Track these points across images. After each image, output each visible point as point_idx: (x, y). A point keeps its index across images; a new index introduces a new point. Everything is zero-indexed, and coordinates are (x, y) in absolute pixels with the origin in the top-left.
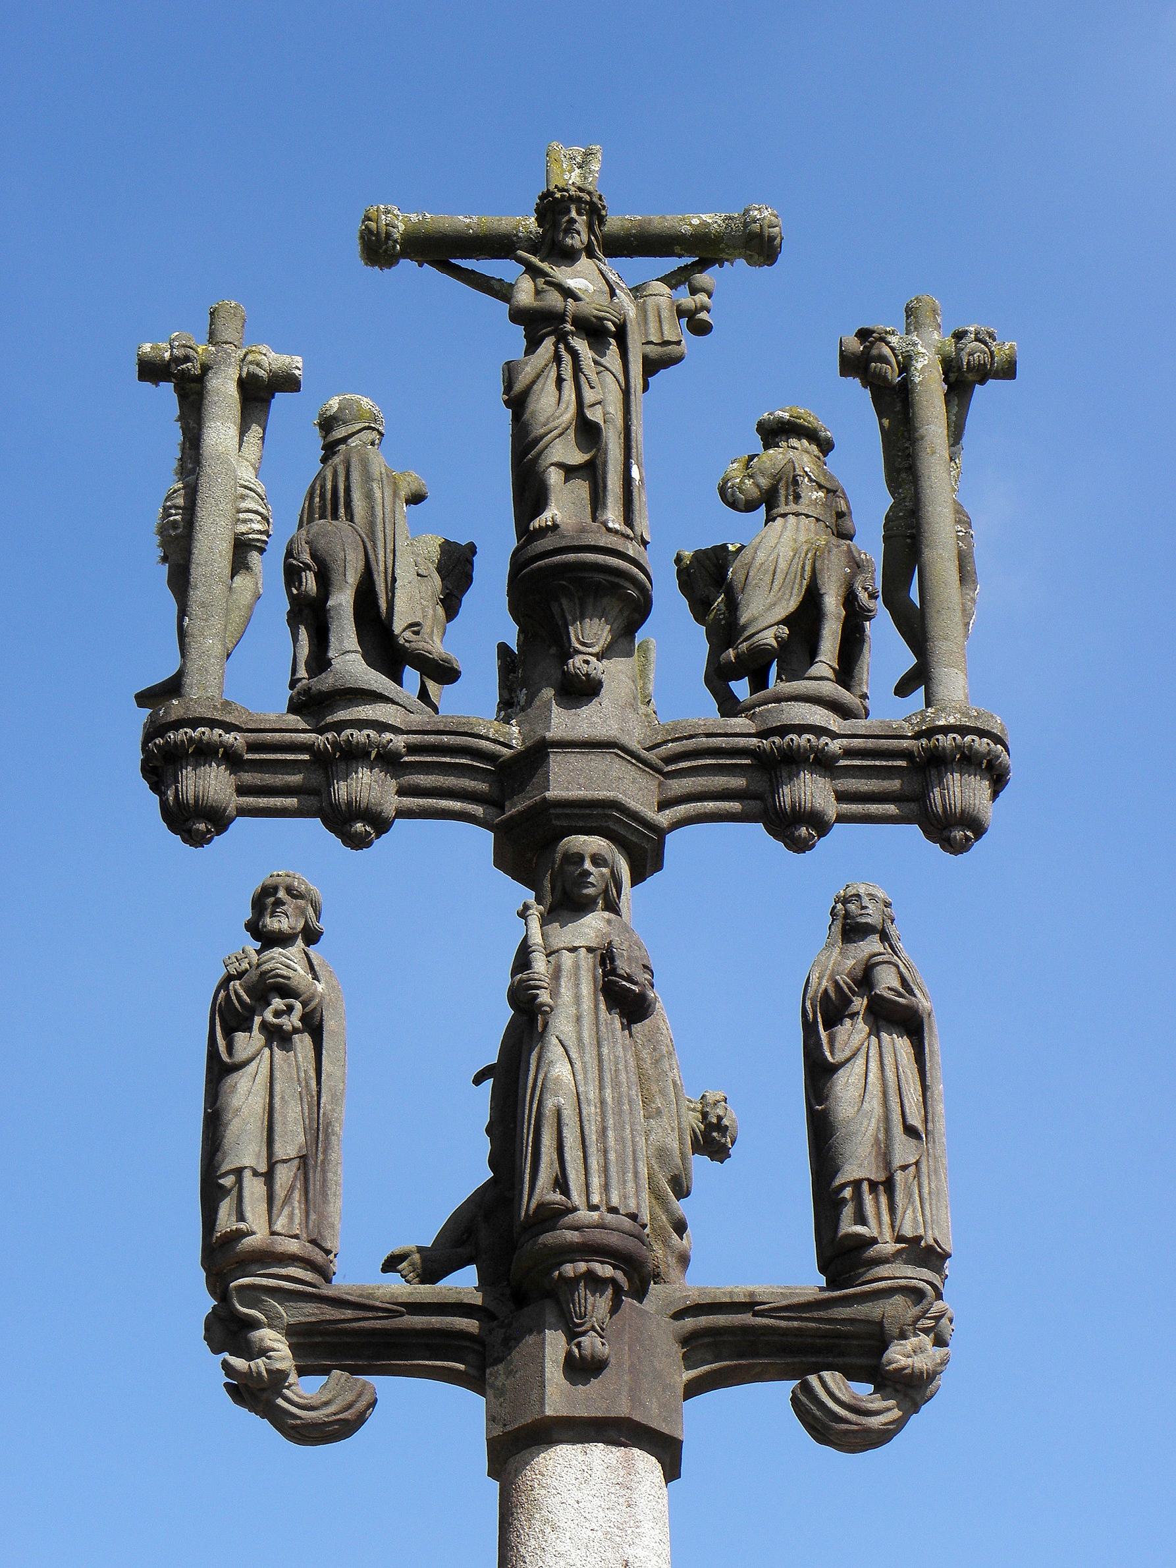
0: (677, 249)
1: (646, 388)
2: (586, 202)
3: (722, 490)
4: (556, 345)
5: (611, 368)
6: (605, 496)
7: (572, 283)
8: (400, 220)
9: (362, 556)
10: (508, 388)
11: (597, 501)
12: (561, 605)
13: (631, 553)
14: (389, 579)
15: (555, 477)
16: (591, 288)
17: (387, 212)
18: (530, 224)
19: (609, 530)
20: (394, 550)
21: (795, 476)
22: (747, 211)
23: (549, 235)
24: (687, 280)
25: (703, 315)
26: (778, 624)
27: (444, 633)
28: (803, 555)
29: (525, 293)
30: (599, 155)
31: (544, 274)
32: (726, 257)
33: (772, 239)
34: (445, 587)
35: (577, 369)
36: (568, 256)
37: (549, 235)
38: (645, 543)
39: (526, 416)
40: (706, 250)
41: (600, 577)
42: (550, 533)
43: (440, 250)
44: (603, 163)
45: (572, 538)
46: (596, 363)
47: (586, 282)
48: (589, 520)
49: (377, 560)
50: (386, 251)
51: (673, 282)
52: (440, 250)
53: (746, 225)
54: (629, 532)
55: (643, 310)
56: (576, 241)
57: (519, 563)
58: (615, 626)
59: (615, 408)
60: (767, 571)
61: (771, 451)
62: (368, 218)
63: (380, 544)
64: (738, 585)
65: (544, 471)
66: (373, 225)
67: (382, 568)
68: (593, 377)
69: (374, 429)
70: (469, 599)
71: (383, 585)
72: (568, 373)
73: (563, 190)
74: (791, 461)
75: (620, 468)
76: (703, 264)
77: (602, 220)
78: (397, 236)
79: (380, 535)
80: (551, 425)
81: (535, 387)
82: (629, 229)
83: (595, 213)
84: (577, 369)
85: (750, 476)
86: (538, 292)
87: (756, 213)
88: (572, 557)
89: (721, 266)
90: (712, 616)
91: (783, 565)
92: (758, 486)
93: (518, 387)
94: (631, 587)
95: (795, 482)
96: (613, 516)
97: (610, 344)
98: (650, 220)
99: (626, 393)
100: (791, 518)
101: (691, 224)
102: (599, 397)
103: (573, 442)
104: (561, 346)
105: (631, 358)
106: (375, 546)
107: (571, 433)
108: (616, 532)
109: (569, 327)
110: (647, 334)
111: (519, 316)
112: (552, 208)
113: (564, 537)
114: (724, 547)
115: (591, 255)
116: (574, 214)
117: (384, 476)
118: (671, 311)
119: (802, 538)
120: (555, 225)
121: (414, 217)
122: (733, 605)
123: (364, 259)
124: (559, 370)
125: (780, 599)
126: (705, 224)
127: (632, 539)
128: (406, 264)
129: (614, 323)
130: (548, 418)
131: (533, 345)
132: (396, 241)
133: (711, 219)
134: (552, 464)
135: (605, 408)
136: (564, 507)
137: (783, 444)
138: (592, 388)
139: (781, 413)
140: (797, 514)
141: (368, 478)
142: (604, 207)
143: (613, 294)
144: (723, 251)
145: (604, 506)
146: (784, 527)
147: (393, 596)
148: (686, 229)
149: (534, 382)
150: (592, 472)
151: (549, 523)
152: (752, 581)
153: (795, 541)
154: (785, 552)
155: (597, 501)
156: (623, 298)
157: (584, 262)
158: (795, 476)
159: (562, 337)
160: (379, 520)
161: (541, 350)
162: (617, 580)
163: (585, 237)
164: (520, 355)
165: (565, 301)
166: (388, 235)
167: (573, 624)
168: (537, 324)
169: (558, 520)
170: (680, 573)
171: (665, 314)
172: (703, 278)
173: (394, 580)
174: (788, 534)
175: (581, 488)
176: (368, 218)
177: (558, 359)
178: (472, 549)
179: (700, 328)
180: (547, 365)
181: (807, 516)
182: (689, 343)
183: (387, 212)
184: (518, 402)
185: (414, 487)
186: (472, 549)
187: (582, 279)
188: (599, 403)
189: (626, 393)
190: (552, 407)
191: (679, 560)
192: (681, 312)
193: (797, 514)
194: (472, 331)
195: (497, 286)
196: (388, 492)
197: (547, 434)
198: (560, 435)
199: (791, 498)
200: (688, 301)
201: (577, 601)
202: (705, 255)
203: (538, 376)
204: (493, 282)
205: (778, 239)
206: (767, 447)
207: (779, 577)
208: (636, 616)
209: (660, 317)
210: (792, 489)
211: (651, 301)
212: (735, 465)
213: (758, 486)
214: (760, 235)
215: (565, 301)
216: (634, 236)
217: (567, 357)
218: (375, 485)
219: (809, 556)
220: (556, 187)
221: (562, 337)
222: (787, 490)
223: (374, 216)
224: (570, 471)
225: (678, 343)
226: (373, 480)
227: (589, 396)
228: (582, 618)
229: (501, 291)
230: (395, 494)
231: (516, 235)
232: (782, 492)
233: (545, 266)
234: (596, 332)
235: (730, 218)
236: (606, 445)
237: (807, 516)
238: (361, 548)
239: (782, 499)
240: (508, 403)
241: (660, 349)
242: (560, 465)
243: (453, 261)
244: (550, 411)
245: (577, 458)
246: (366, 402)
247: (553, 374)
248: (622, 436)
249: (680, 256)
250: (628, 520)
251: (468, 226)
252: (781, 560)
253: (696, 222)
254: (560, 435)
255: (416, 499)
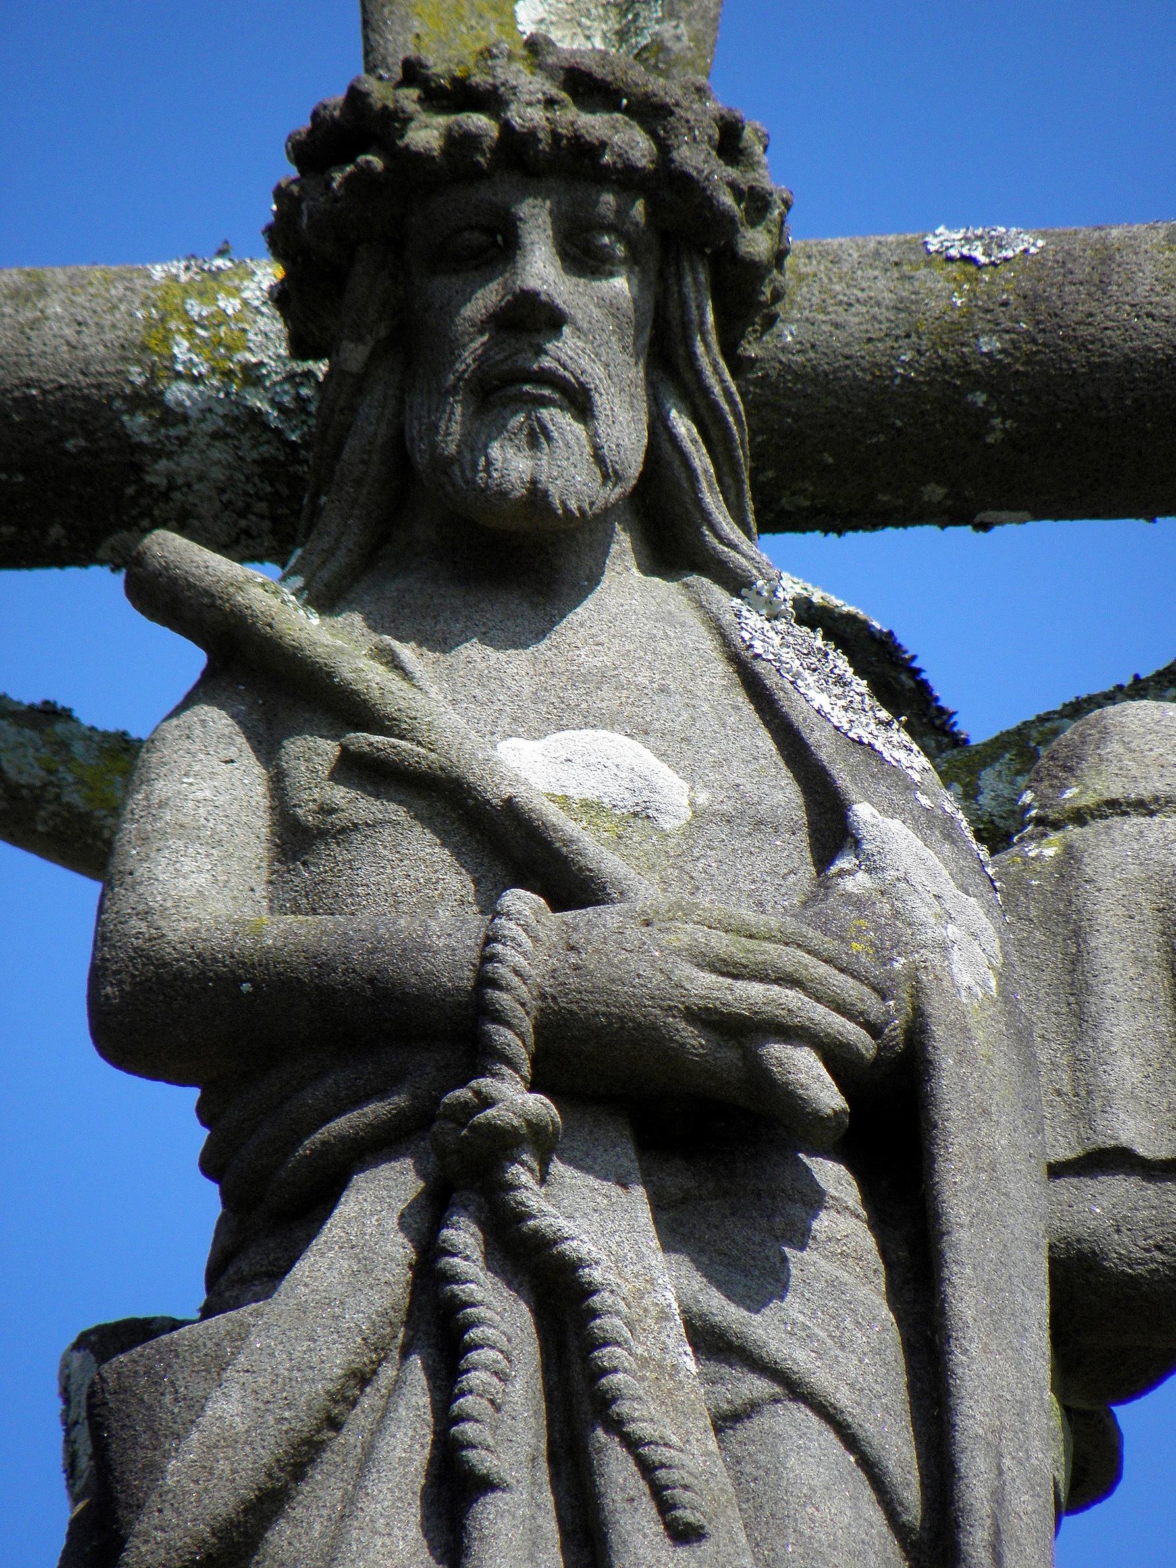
1: (1092, 1470)
2: (627, 179)
4: (426, 1224)
5: (822, 1379)
7: (533, 768)
16: (675, 796)
18: (225, 312)
29: (207, 849)
35: (578, 1400)
36: (516, 569)
46: (710, 1341)
55: (1055, 931)
56: (565, 462)
68: (692, 1454)
73: (459, 95)
77: (744, 296)
82: (956, 330)
83: (693, 245)
84: (578, 1400)
86: (296, 838)
97: (815, 1200)
98: (1105, 256)
104: (464, 1236)
109: (514, 1099)
110: (1085, 1099)
111: (153, 1012)
112: (392, 219)
115: (673, 546)
116: (541, 268)
120: (412, 345)
124: (445, 1417)
129: (836, 1057)
131: (266, 1220)
138: (684, 1534)
142: (757, 204)
143: (831, 831)
156: (910, 845)
159: (468, 1176)
161: (321, 1266)
163: (624, 428)
165: (489, 906)
177: (437, 1327)
180: (362, 1378)
187: (619, 725)
203: (302, 1458)
215: (489, 906)
216: (995, 376)
217: (502, 1319)
220: (413, 73)
221: (468, 1176)
233: (338, 641)
234: (699, 1118)
247: (407, 1445)
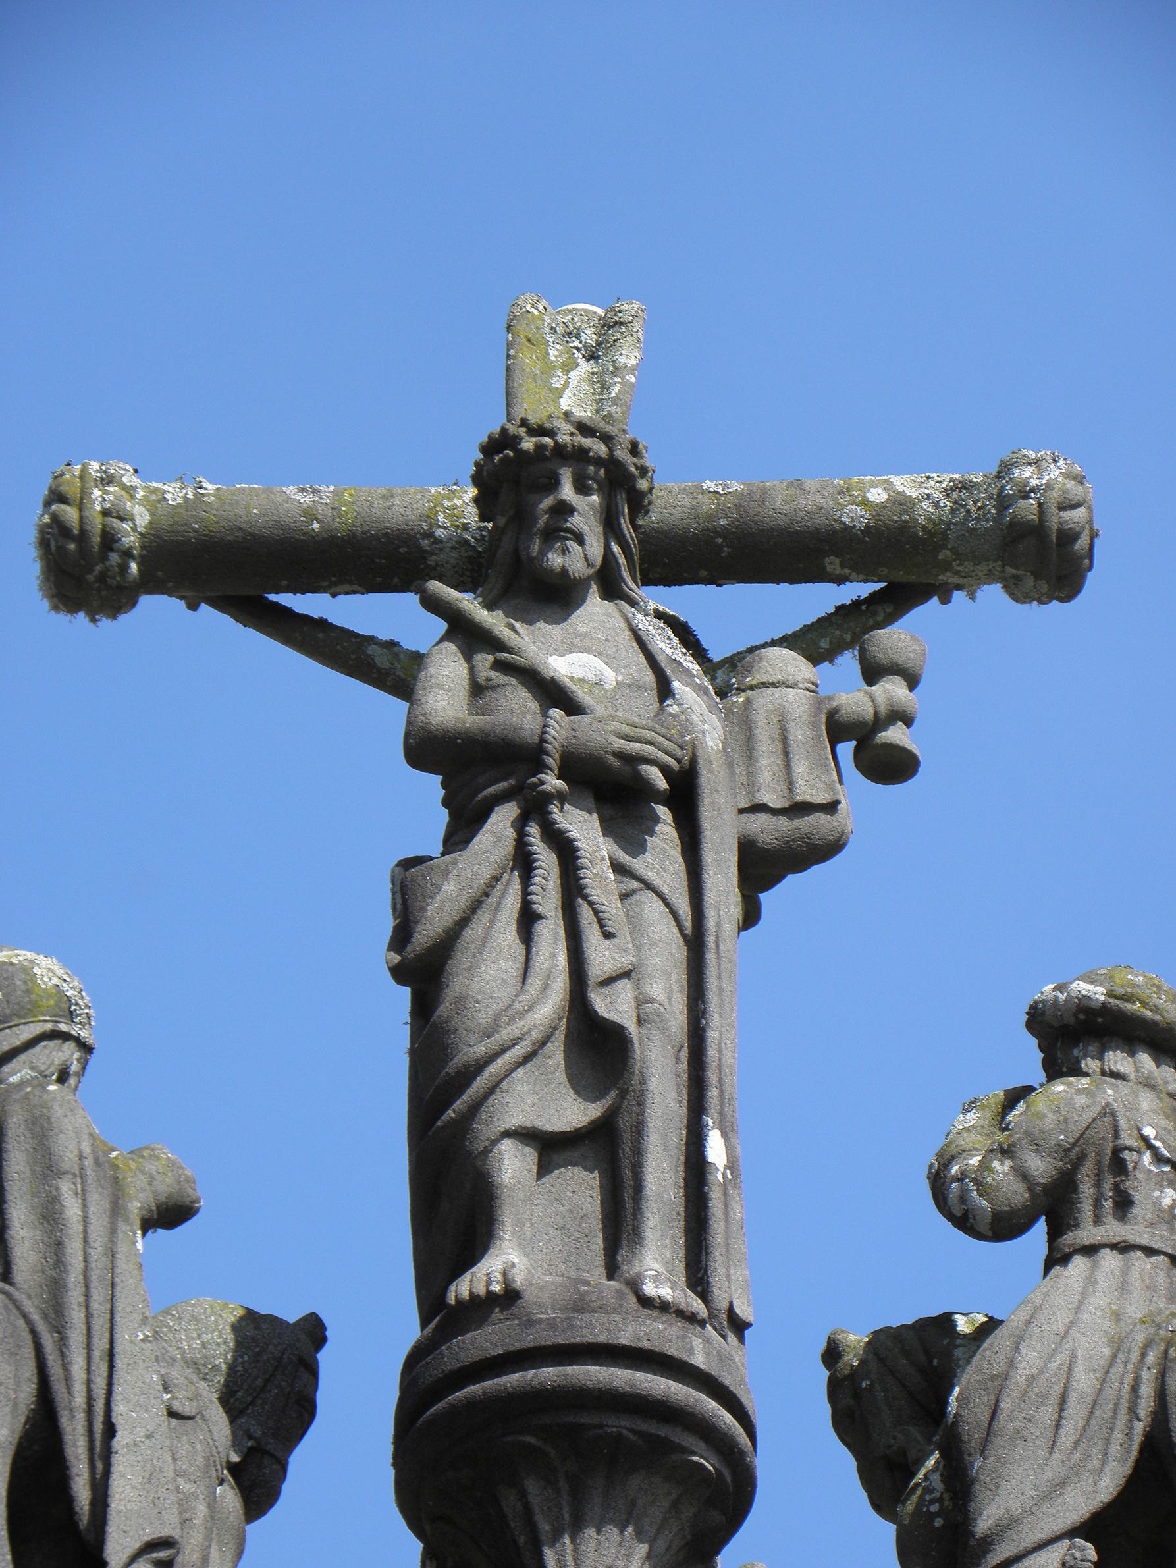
0: (832, 564)
1: (751, 916)
2: (598, 461)
3: (938, 1182)
4: (520, 825)
6: (637, 1211)
7: (564, 666)
8: (140, 496)
9: (29, 1370)
10: (401, 937)
11: (619, 1224)
12: (523, 1494)
13: (699, 1360)
14: (98, 1427)
15: (512, 1165)
16: (610, 677)
17: (107, 480)
18: (457, 505)
19: (646, 1302)
20: (111, 1355)
21: (1117, 1151)
22: (1005, 468)
23: (507, 544)
24: (856, 640)
25: (896, 734)
26: (1072, 1533)
27: (240, 1554)
28: (1135, 1356)
30: (638, 328)
31: (493, 643)
32: (956, 580)
33: (1068, 537)
34: (239, 1434)
36: (554, 597)
37: (507, 544)
38: (739, 1326)
39: (444, 1009)
40: (903, 563)
41: (620, 1424)
42: (497, 1314)
43: (244, 572)
44: (647, 348)
45: (552, 1324)
46: (619, 869)
47: (597, 663)
48: (598, 1274)
49: (69, 1387)
50: (103, 577)
51: (824, 644)
52: (244, 572)
53: (1003, 502)
54: (697, 1306)
55: (742, 728)
56: (574, 560)
57: (423, 1391)
58: (661, 1544)
59: (666, 987)
60: (1043, 1398)
61: (1059, 1087)
62: (62, 499)
63: (76, 1338)
64: (971, 1432)
65: (487, 1151)
66: (70, 514)
67: (80, 1400)
68: (612, 908)
69: (66, 1037)
70: (306, 1461)
71: (82, 1442)
72: (548, 899)
73: (541, 431)
74: (1108, 1112)
75: (677, 1137)
76: (897, 600)
77: (638, 503)
78: (130, 540)
79: (76, 1316)
80: (505, 1034)
81: (468, 934)
82: (712, 517)
83: (621, 484)
84: (572, 888)
85: (1005, 1152)
86: (478, 689)
87: (1028, 472)
88: (549, 1375)
89: (945, 600)
90: (910, 1506)
91: (1084, 1381)
92: (1023, 1175)
93: (426, 933)
94: (700, 1446)
95: (1119, 1166)
96: (658, 1266)
99: (696, 944)
100: (1106, 1253)
101: (865, 503)
102: (626, 960)
103: (561, 1075)
104: (533, 830)
105: (709, 855)
106: (62, 1343)
107: (556, 1051)
108: (663, 1307)
109: (552, 782)
110: (752, 786)
111: (426, 749)
112: (515, 472)
113: (531, 1323)
114: (945, 1321)
115: (611, 589)
116: (567, 492)
117: (88, 1162)
118: (814, 725)
119: (1135, 1309)
120: (522, 518)
121: (174, 493)
122: (959, 1484)
123: (51, 597)
124: (526, 893)
125: (1077, 1471)
126: (901, 502)
127: (702, 1323)
128: (158, 611)
129: (665, 770)
130: (498, 1016)
131: (464, 825)
132: (127, 554)
133: (914, 485)
134: (507, 1134)
135: (643, 989)
136: (534, 1245)
137: (1090, 1064)
138: (608, 936)
139: (1084, 987)
140: (1123, 1248)
141: (47, 1168)
142: (643, 471)
143: (664, 690)
144: (946, 566)
145: (636, 1237)
146: (1090, 1281)
147: (107, 1472)
148: (853, 515)
149: (463, 922)
150: (606, 1147)
151: (496, 1288)
152: (1008, 1423)
153: (1117, 1316)
154: (1091, 1345)
155: (619, 1224)
156: (692, 696)
157: (595, 610)
158: (1117, 1151)
159: (535, 808)
160: (74, 1277)
162: (663, 1431)
164: (434, 847)
165: (545, 714)
166: (109, 540)
167: (555, 1539)
168: (473, 771)
169: (519, 1279)
170: (835, 1388)
171: (799, 734)
172: (897, 638)
173: (110, 1431)
174: (1100, 1300)
175: (581, 1187)
176: (57, 496)
177: (524, 862)
178: (314, 1331)
179: (890, 767)
180: (497, 879)
181: (1150, 1251)
182: (860, 801)
183: (107, 480)
184: (424, 970)
185: (165, 1187)
186: (314, 1331)
187: (588, 654)
188: (626, 975)
189: (696, 944)
190: (508, 987)
191: (832, 1354)
192: (838, 728)
193: (1123, 1248)
194: (311, 769)
195: (382, 660)
196: (99, 1204)
197: (504, 1050)
198: (527, 1059)
199: (1108, 1205)
200: (857, 700)
201: (563, 1484)
202: (901, 576)
203: (475, 906)
204: (372, 650)
205: (1084, 540)
206: (1055, 1069)
207: (1075, 1412)
208: (716, 1517)
209: (784, 740)
210: (1109, 1181)
211: (764, 701)
212: (972, 1117)
213: (1023, 1175)
214: (1036, 531)
215: (545, 714)
216: (725, 533)
217: (546, 859)
218: (66, 1188)
219: (1151, 1357)
220: (524, 423)
221: (535, 808)
222: (1098, 1184)
223: (73, 491)
224: (550, 1148)
225: (831, 807)
226: (60, 1174)
227: (602, 957)
228: (576, 1527)
229: (393, 671)
230: (116, 1209)
231: (429, 535)
232: (1086, 1189)
233: (493, 620)
234: (615, 791)
235: (963, 486)
236: (643, 1082)
237: (1150, 1251)
238: (28, 1352)
239: (1087, 1207)
240: (400, 973)
241: (784, 825)
242: (527, 1135)
243: (272, 597)
244: (503, 996)
245: (571, 1112)
246: (48, 971)
247: (512, 903)
248: (684, 1054)
249: (840, 580)
250: (698, 1275)
251: (310, 514)
252: (1079, 1370)
253: (877, 495)
254: (527, 1059)
255: (171, 1214)
